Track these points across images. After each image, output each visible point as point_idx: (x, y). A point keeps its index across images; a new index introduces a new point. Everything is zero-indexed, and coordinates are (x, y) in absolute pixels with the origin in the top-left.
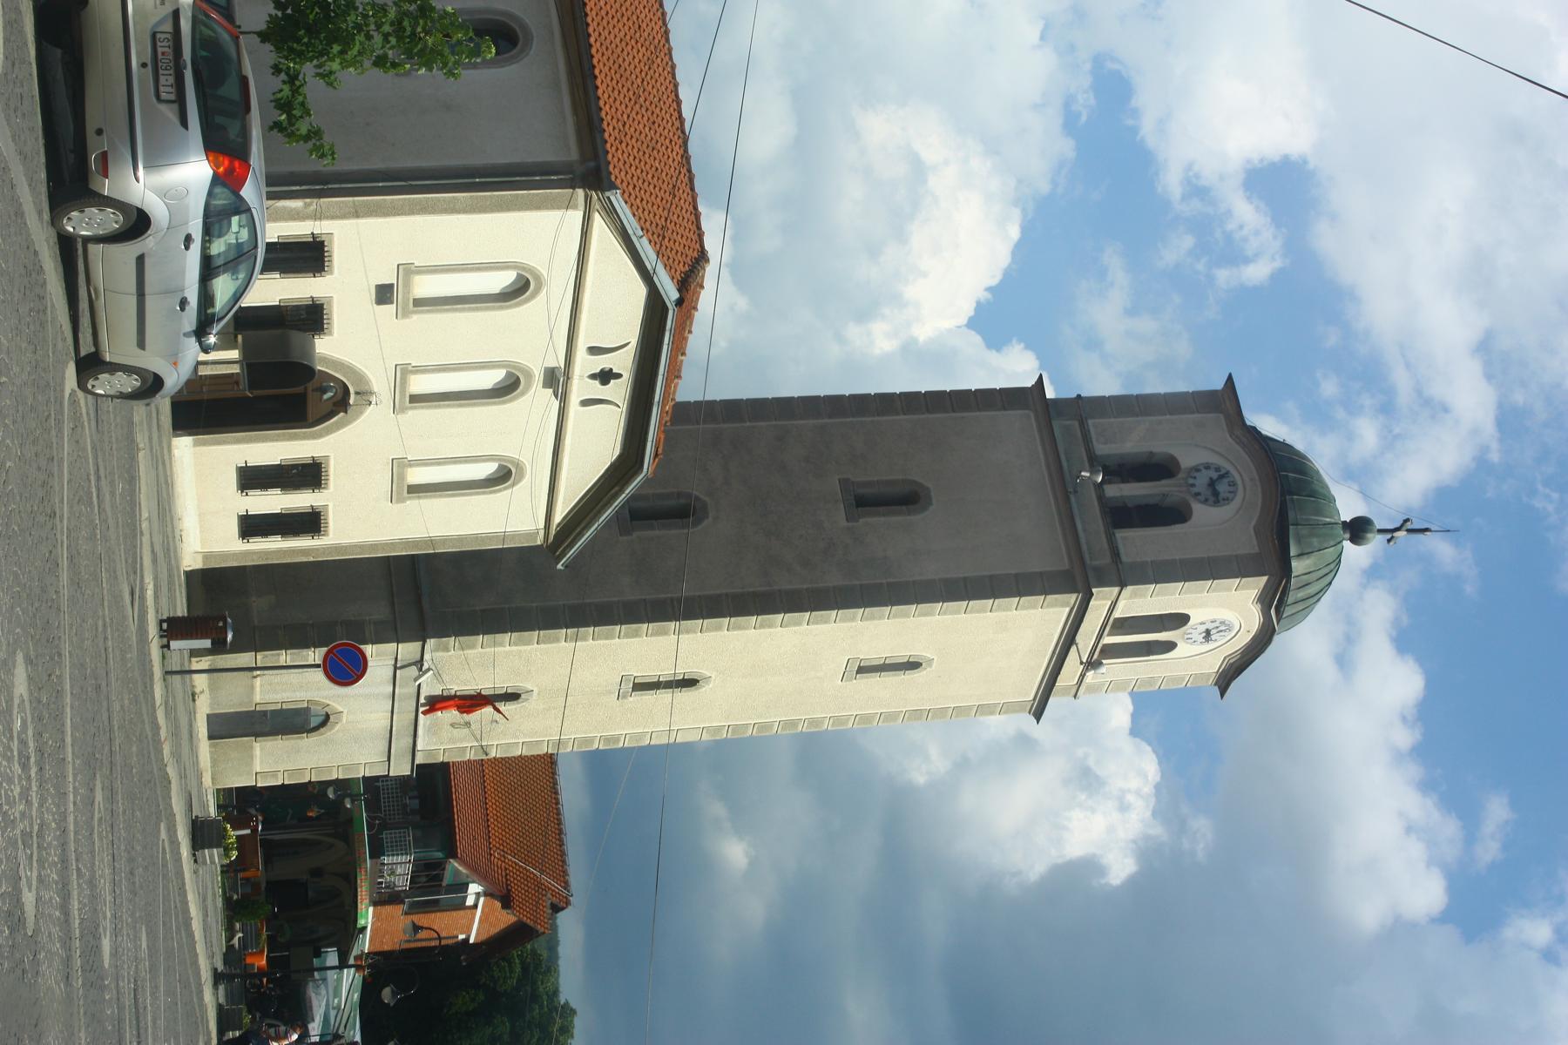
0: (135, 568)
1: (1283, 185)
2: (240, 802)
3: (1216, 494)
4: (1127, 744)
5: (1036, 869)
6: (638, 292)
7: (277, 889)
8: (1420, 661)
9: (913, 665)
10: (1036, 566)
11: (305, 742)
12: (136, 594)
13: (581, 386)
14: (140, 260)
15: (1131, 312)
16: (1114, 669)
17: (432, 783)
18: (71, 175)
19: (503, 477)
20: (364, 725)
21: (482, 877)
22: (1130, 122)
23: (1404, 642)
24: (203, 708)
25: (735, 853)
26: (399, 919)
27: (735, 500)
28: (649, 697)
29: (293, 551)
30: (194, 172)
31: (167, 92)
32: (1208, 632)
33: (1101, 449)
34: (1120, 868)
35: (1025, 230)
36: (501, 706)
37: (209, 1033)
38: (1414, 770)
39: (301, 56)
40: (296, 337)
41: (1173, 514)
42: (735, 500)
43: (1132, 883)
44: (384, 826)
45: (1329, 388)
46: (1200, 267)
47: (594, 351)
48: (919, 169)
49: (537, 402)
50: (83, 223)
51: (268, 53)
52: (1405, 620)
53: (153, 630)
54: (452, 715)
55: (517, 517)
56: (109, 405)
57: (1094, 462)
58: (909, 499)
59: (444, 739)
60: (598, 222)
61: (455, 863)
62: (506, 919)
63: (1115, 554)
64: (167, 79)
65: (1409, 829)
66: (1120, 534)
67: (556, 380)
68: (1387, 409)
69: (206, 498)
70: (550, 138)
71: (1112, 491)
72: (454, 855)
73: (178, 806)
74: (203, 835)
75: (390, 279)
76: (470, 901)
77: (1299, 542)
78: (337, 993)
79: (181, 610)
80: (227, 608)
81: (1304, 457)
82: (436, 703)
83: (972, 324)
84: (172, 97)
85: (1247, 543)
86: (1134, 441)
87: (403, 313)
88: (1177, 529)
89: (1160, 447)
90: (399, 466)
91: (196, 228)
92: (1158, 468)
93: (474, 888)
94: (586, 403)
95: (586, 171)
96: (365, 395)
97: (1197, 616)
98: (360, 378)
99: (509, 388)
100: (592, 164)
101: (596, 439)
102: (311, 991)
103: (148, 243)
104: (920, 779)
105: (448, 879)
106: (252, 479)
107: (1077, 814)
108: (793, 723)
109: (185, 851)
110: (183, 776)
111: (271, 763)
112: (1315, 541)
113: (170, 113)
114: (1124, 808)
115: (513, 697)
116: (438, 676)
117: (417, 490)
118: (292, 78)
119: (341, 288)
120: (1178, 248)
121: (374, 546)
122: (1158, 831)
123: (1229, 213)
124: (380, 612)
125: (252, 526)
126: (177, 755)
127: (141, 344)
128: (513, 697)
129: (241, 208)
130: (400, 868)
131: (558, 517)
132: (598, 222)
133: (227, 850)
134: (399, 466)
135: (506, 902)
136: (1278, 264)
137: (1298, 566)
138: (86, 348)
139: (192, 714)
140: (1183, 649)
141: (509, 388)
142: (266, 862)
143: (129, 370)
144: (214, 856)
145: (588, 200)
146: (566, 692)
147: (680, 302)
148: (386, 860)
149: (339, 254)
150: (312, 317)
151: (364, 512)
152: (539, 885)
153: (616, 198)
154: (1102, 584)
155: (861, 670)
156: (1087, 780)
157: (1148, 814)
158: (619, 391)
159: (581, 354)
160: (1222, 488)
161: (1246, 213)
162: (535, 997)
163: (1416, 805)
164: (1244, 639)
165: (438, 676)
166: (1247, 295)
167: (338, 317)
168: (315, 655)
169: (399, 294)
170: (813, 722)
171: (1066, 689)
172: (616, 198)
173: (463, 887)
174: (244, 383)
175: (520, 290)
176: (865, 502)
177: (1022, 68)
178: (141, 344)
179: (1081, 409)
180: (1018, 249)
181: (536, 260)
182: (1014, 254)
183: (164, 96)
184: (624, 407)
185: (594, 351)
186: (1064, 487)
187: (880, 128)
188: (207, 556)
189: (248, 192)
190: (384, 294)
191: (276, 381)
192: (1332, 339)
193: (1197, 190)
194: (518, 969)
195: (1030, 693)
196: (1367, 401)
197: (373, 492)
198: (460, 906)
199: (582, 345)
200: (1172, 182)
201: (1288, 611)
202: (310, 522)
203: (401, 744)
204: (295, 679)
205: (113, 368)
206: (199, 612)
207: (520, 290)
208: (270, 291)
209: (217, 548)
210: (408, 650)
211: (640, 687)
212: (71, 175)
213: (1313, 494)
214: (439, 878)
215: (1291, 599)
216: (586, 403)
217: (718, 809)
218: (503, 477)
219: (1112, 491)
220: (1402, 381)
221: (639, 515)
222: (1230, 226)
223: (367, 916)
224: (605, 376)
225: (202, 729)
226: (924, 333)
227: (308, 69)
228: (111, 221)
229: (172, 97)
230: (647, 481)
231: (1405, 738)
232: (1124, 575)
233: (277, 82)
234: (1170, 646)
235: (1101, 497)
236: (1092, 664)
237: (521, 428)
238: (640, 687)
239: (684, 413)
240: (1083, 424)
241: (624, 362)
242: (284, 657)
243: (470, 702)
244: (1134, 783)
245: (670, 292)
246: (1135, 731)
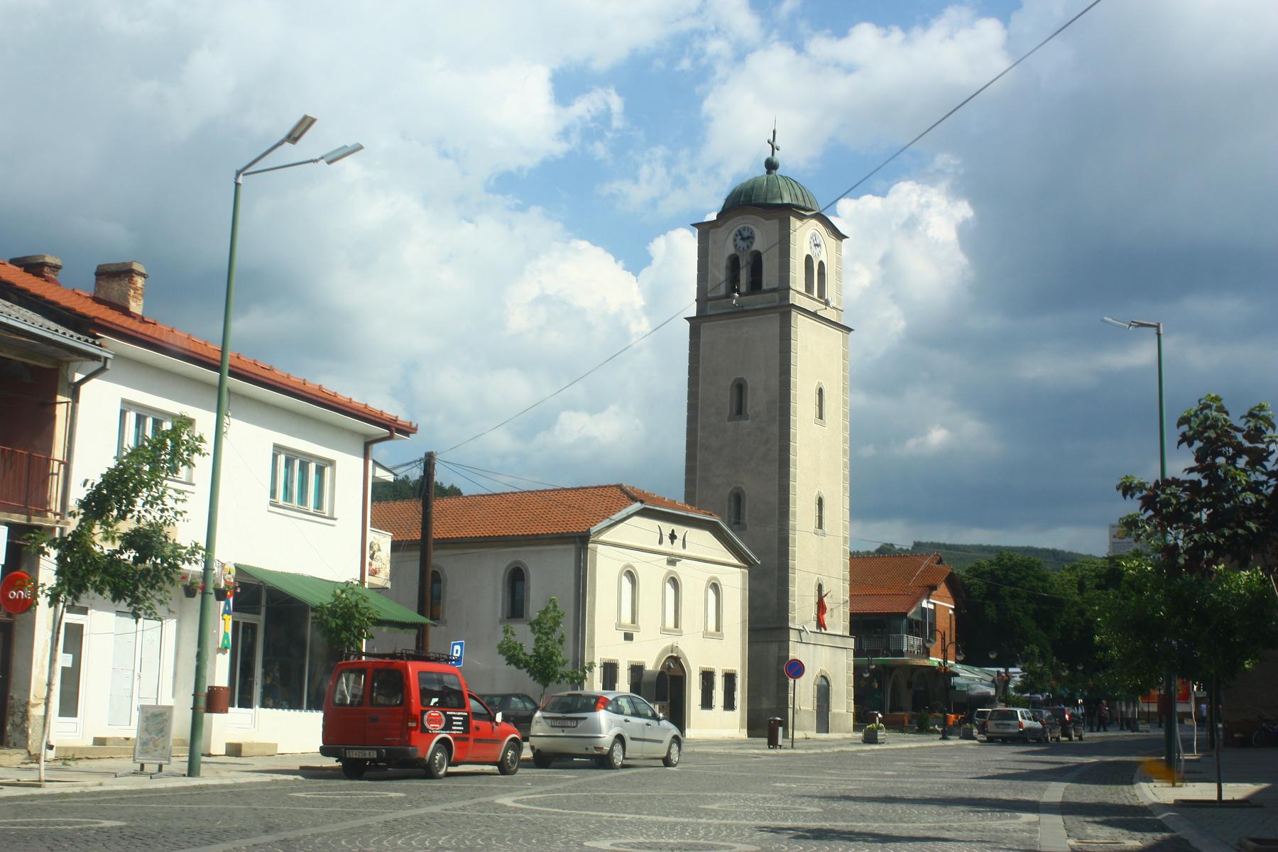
0: (745, 756)
1: (568, 85)
2: (862, 718)
3: (748, 238)
4: (892, 198)
5: (961, 259)
6: (636, 520)
7: (916, 706)
8: (853, 25)
9: (821, 392)
11: (834, 688)
12: (757, 756)
13: (677, 548)
14: (632, 739)
15: (636, 180)
16: (830, 293)
17: (862, 625)
18: (602, 761)
19: (715, 587)
20: (825, 658)
21: (919, 599)
22: (525, 173)
23: (841, 32)
24: (813, 734)
25: (937, 436)
26: (936, 646)
27: (731, 470)
28: (825, 521)
29: (742, 693)
30: (603, 716)
32: (817, 245)
33: (722, 291)
34: (964, 210)
35: (582, 238)
36: (824, 593)
37: (1151, 761)
38: (916, 31)
39: (555, 673)
40: (645, 678)
41: (757, 260)
42: (731, 470)
43: (973, 204)
44: (888, 649)
45: (685, 64)
46: (609, 135)
47: (661, 542)
48: (543, 299)
49: (681, 569)
50: (618, 758)
51: (552, 685)
52: (828, 31)
53: (773, 752)
54: (826, 617)
55: (735, 581)
56: (682, 758)
57: (728, 296)
58: (740, 387)
59: (839, 621)
61: (910, 614)
62: (943, 589)
63: (774, 290)
64: (569, 723)
65: (951, 37)
66: (765, 287)
68: (701, 34)
69: (716, 725)
70: (563, 558)
71: (743, 289)
72: (905, 614)
73: (854, 748)
74: (870, 739)
76: (932, 607)
77: (774, 198)
78: (973, 679)
79: (766, 740)
80: (767, 721)
81: (733, 192)
82: (820, 624)
83: (636, 273)
85: (773, 225)
86: (719, 274)
90: (706, 634)
91: (621, 718)
92: (734, 263)
93: (924, 604)
94: (684, 546)
95: (581, 541)
96: (673, 649)
98: (665, 651)
99: (675, 582)
101: (702, 542)
102: (973, 693)
103: (626, 736)
104: (902, 324)
105: (918, 618)
106: (707, 703)
107: (930, 233)
108: (844, 451)
109: (876, 747)
110: (841, 745)
111: (843, 705)
112: (775, 190)
113: (581, 723)
114: (928, 205)
115: (820, 587)
116: (806, 623)
117: (718, 628)
118: (562, 676)
119: (625, 657)
120: (600, 150)
121: (743, 649)
122: (944, 185)
123: (580, 118)
124: (774, 648)
125: (729, 704)
126: (830, 747)
127: (661, 742)
128: (820, 587)
129: (616, 699)
130: (911, 642)
131: (736, 562)
132: (603, 538)
133: (879, 728)
134: (706, 634)
135: (933, 588)
136: (612, 91)
137: (787, 200)
138: (661, 763)
139: (815, 740)
140: (823, 258)
141: (675, 582)
142: (901, 710)
143: (670, 747)
144: (881, 735)
145: (594, 542)
146: (820, 561)
147: (642, 502)
148: (905, 649)
149: (610, 656)
150: (636, 670)
152: (926, 570)
153: (594, 529)
154: (788, 298)
155: (821, 417)
156: (911, 224)
157: (932, 190)
158: (680, 530)
160: (746, 234)
161: (581, 108)
162: (992, 573)
163: (937, 31)
165: (806, 623)
166: (628, 111)
167: (637, 659)
168: (791, 681)
169: (629, 631)
170: (844, 442)
171: (838, 316)
172: (594, 529)
173: (924, 610)
174: (664, 703)
175: (631, 576)
176: (739, 411)
177: (489, 235)
178: (661, 742)
179: (702, 299)
180: (595, 244)
181: (618, 567)
182: (595, 245)
184: (687, 529)
185: (661, 542)
186: (741, 312)
187: (518, 321)
188: (742, 727)
189: (610, 697)
191: (665, 689)
192: (660, 63)
193: (565, 134)
194: (976, 580)
195: (838, 334)
196: (697, 45)
197: (719, 648)
198: (933, 612)
200: (560, 148)
201: (809, 206)
202: (730, 678)
203: (838, 642)
204: (803, 693)
205: (669, 753)
206: (767, 733)
207: (631, 576)
208: (623, 685)
209: (738, 721)
210: (793, 636)
211: (820, 526)
212: (602, 761)
213: (752, 189)
214: (917, 622)
215: (802, 204)
216: (684, 546)
217: (911, 443)
218: (715, 587)
219: (743, 289)
220: (687, 25)
221: (737, 520)
222: (588, 117)
223: (935, 661)
224: (673, 537)
225: (823, 736)
226: (639, 301)
227: (560, 670)
228: (618, 747)
230: (723, 520)
231: (897, 35)
232: (784, 288)
233: (564, 682)
234: (821, 264)
235: (746, 294)
236: (827, 303)
237: (693, 577)
238: (820, 526)
239: (690, 498)
241: (667, 528)
242: (791, 695)
243: (821, 608)
244: (914, 197)
245: (637, 506)
246: (884, 194)
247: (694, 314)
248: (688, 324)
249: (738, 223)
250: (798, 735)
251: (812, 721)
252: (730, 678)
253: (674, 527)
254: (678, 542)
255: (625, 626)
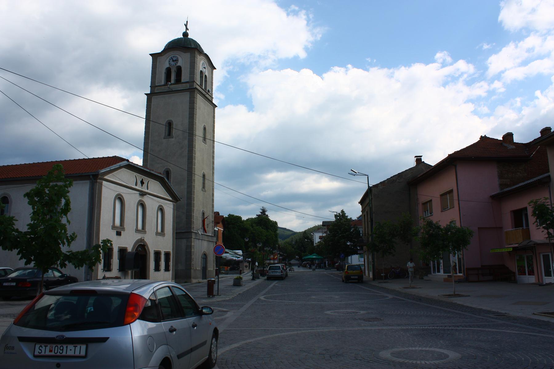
3: (176, 60)
9: (205, 129)
10: (187, 106)
11: (209, 259)
24: (201, 280)
28: (206, 185)
31: (81, 350)
33: (163, 83)
41: (179, 70)
47: (136, 185)
49: (147, 200)
55: (169, 208)
58: (170, 124)
60: (106, 177)
62: (221, 224)
66: (183, 81)
67: (143, 194)
71: (173, 82)
75: (114, 232)
84: (84, 347)
85: (188, 55)
87: (124, 229)
88: (183, 69)
89: (164, 71)
90: (157, 234)
96: (142, 240)
97: (201, 69)
98: (138, 241)
99: (142, 205)
100: (91, 177)
101: (155, 187)
106: (157, 269)
115: (203, 214)
116: (198, 230)
119: (117, 243)
124: (184, 241)
125: (167, 269)
128: (203, 214)
131: (171, 199)
132: (106, 177)
134: (157, 234)
135: (219, 223)
150: (122, 251)
151: (164, 244)
158: (146, 179)
159: (137, 187)
160: (174, 59)
164: (206, 61)
176: (169, 134)
181: (114, 195)
183: (83, 353)
184: (149, 179)
185: (136, 185)
188: (172, 279)
190: (119, 234)
198: (218, 231)
199: (135, 187)
202: (167, 254)
203: (210, 239)
218: (161, 209)
219: (173, 82)
229: (84, 347)
234: (206, 76)
237: (152, 204)
240: (157, 86)
241: (140, 177)
247: (149, 92)
248: (146, 97)
249: (171, 54)
250: (194, 281)
251: (200, 274)
252: (167, 254)
253: (143, 177)
254: (145, 185)
255: (117, 227)
